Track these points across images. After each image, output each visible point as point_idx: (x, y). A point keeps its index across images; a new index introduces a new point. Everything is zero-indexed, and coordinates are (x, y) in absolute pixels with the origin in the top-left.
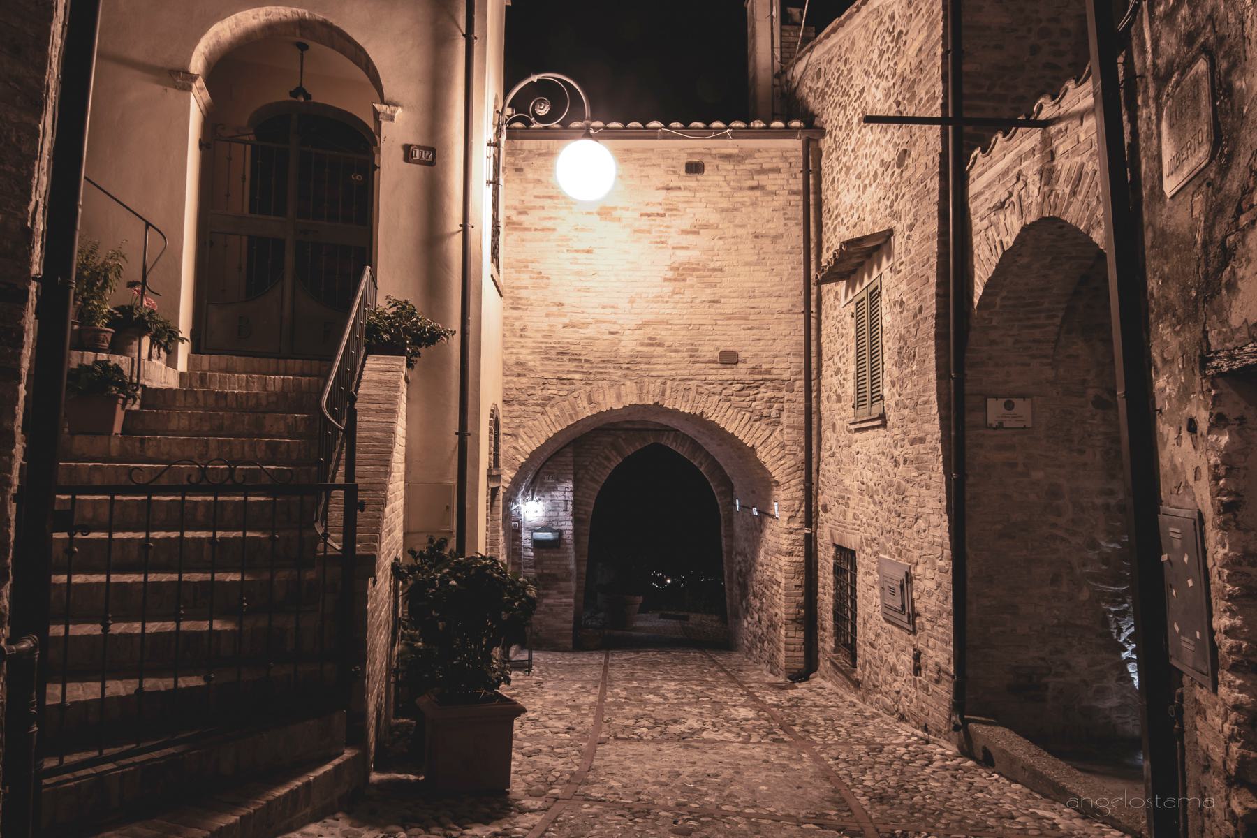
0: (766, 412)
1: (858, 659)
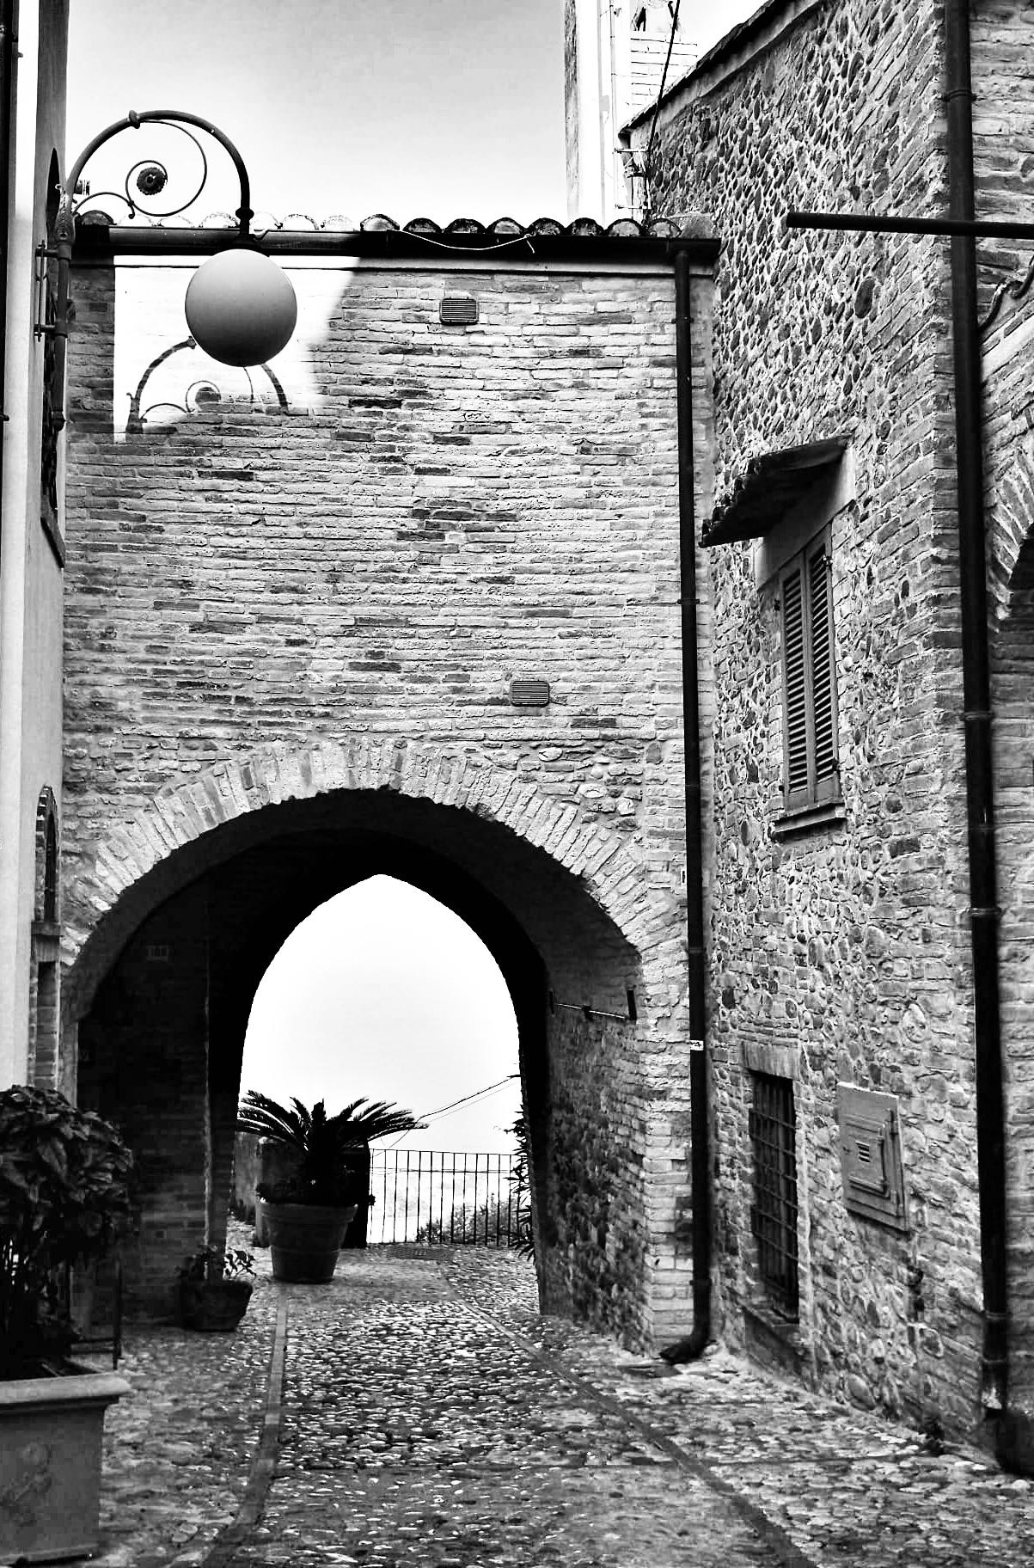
0: (607, 804)
1: (801, 1302)
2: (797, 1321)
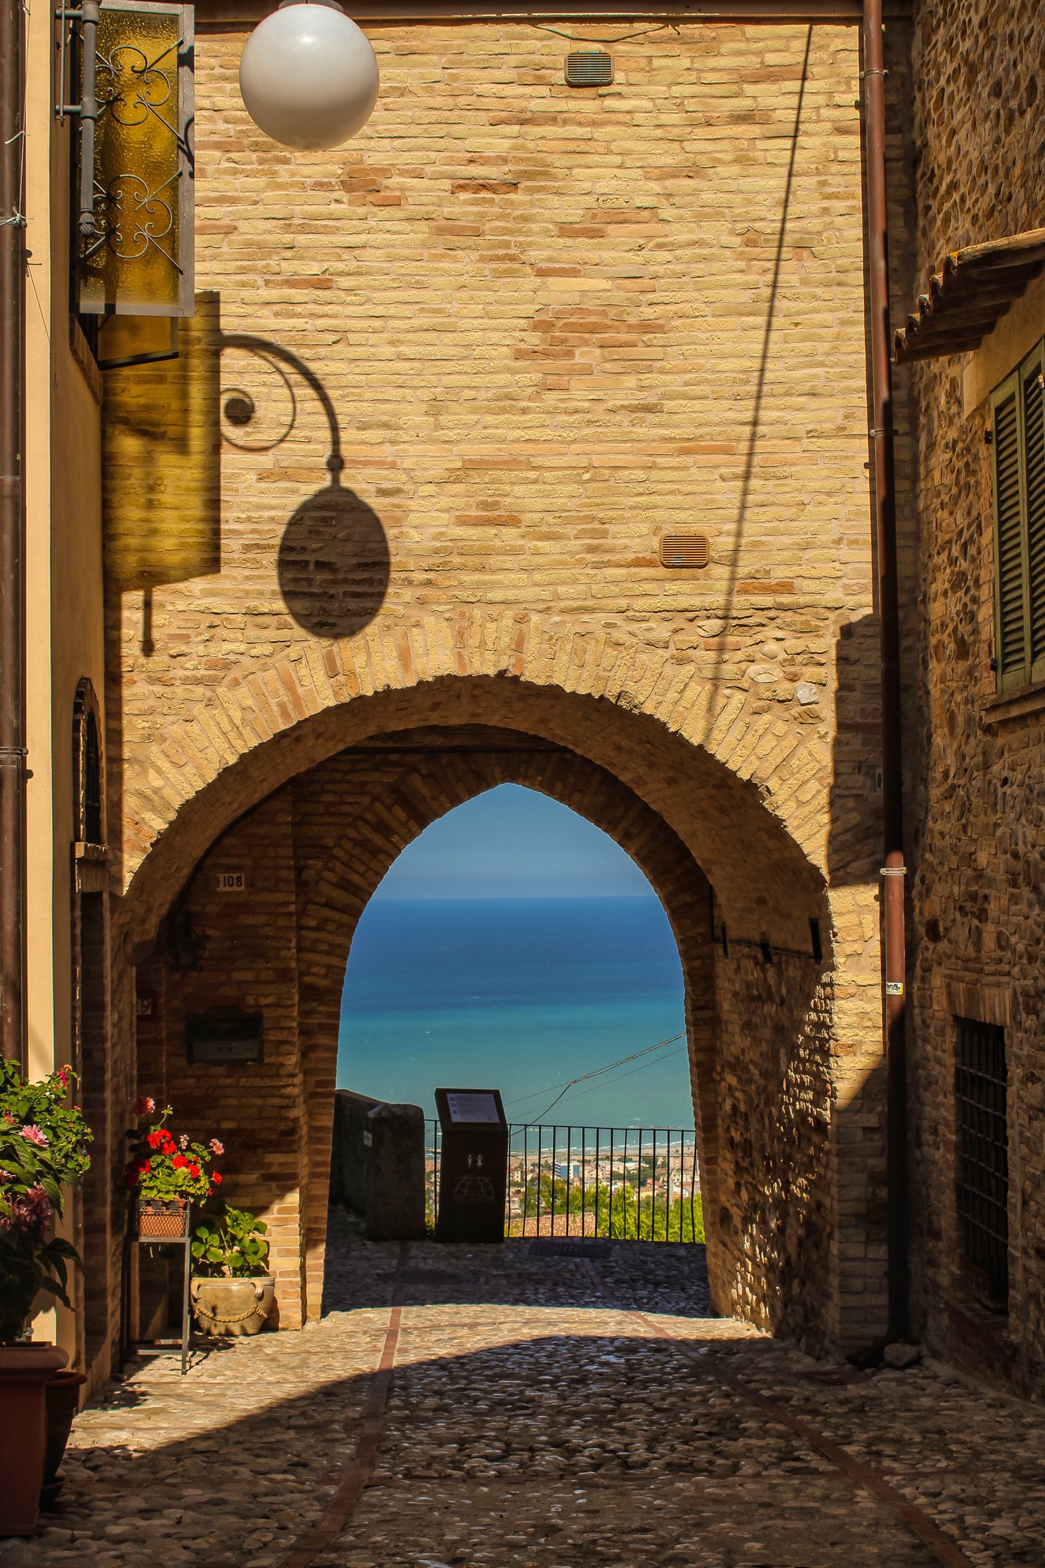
0: (784, 689)
1: (1012, 1292)
2: (1005, 1312)
